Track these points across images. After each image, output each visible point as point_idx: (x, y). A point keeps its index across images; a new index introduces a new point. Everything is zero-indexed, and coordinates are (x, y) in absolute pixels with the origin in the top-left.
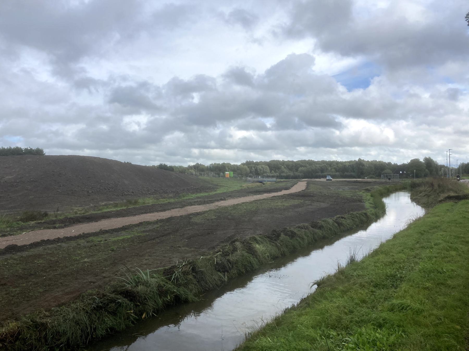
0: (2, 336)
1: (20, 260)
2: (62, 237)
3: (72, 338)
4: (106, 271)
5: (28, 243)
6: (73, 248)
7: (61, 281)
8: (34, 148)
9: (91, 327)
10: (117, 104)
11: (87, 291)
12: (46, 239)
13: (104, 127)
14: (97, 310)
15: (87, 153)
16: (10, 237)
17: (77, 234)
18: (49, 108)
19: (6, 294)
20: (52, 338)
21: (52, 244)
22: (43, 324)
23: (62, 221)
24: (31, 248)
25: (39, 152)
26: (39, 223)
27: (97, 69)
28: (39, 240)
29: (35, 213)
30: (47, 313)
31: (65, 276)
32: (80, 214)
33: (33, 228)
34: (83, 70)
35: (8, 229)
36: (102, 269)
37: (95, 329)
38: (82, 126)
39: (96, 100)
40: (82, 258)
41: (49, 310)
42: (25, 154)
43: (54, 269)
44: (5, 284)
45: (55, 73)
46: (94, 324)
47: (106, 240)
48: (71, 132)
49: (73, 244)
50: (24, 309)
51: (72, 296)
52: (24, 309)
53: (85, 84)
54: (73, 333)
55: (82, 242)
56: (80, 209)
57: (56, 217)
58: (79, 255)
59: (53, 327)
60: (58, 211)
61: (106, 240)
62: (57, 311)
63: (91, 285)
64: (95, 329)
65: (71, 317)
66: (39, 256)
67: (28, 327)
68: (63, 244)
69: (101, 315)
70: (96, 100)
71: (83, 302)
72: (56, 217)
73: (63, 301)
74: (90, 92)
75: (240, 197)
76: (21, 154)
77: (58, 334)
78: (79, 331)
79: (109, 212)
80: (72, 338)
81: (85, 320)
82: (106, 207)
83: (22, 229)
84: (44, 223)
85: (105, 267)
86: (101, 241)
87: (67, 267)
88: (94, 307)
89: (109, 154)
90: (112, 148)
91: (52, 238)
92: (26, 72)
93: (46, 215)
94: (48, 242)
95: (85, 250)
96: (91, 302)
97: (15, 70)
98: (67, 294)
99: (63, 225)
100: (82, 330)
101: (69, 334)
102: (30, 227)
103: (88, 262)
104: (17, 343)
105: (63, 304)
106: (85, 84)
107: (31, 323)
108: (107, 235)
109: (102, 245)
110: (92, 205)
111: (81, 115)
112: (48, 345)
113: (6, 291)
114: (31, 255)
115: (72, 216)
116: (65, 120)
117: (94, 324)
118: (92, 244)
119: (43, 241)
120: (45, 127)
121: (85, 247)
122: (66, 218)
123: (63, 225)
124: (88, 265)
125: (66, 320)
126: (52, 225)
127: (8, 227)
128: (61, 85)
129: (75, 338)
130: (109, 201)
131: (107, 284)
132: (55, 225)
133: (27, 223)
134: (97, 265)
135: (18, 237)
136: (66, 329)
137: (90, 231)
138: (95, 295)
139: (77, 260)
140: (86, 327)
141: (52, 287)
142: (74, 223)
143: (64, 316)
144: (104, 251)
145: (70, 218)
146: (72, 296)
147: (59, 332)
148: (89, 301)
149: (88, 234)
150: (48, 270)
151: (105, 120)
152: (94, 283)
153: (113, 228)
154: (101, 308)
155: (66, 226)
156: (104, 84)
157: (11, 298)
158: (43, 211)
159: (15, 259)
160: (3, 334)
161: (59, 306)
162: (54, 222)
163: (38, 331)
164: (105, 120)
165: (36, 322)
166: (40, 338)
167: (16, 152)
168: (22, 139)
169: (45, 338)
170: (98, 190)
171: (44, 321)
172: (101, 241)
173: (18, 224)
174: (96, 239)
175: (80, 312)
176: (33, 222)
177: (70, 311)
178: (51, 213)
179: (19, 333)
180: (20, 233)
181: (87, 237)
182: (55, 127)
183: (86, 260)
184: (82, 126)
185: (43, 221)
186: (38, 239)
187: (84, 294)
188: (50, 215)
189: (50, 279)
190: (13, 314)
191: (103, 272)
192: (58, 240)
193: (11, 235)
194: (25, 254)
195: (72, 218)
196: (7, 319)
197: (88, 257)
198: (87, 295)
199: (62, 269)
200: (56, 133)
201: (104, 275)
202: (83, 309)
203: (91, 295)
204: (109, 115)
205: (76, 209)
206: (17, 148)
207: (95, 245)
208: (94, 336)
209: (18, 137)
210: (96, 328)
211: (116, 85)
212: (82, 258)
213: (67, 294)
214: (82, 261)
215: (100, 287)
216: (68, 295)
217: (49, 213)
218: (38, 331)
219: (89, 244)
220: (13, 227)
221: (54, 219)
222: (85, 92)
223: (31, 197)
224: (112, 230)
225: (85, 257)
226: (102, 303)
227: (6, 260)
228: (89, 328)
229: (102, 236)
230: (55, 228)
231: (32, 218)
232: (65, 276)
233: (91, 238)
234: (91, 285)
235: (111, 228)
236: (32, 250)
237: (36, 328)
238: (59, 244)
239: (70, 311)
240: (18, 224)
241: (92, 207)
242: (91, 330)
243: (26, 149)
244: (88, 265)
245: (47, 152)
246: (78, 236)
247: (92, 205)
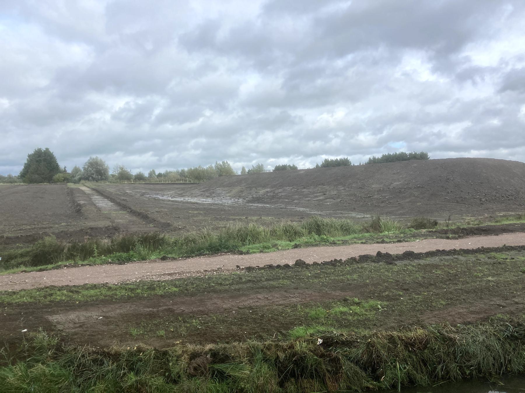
0: (411, 340)
1: (419, 268)
2: (458, 249)
3: (483, 363)
4: (518, 296)
5: (424, 251)
6: (472, 263)
7: (464, 297)
8: (418, 152)
9: (505, 358)
10: (508, 92)
11: (496, 314)
12: (441, 249)
13: (495, 122)
14: (512, 340)
15: (474, 154)
16: (405, 243)
17: (475, 247)
18: (432, 109)
19: (410, 299)
20: (462, 356)
21: (448, 255)
22: (451, 339)
23: (454, 232)
24: (427, 257)
25: (423, 157)
26: (430, 232)
27: (481, 55)
28: (434, 250)
29: (425, 222)
30: (453, 329)
31: (467, 292)
32: (473, 224)
33: (425, 236)
34: (468, 59)
35: (402, 235)
36: (512, 293)
37: (510, 361)
38: (466, 124)
39: (484, 91)
40: (484, 275)
41: (455, 326)
42: (409, 159)
43: (454, 282)
44: (408, 290)
45: (435, 70)
46: (508, 355)
47: (513, 259)
48: (454, 132)
49: (471, 258)
50: (429, 318)
51: (478, 316)
52: (429, 318)
53: (469, 75)
54: (484, 359)
55: (482, 257)
56: (473, 218)
57: (447, 226)
58: (481, 271)
59: (461, 345)
60: (449, 220)
61: (513, 259)
62: (464, 329)
63: (500, 309)
64: (510, 361)
65: (481, 340)
66: (436, 266)
67: (436, 338)
68: (460, 257)
69: (516, 347)
70: (484, 91)
71: (493, 326)
72: (447, 226)
73: (469, 320)
74: (474, 83)
75: (73, 290)
76: (405, 160)
77: (467, 355)
78: (491, 359)
79: (510, 225)
80: (483, 363)
81: (498, 348)
82: (505, 219)
83: (415, 236)
84: (435, 232)
85: (516, 291)
86: (507, 259)
87: (468, 283)
88: (507, 335)
89: (502, 154)
90: (507, 147)
91: (448, 249)
92: (406, 74)
93: (436, 223)
94: (443, 252)
95: (486, 266)
96: (503, 328)
97: (398, 75)
98: (472, 313)
99: (457, 236)
100: (494, 358)
101: (480, 358)
102: (422, 235)
103: (492, 281)
104: (426, 351)
105: (469, 323)
106: (469, 75)
107: (439, 334)
108: (513, 252)
109: (508, 263)
110: (486, 215)
111: (466, 111)
112: (457, 363)
113: (409, 296)
114: (428, 265)
115: (465, 227)
116: (447, 119)
117: (508, 355)
118: (495, 260)
119: (438, 251)
120: (426, 130)
121: (486, 264)
122: (459, 228)
123: (457, 236)
124: (493, 285)
125: (476, 341)
126: (444, 234)
127: (401, 233)
128: (442, 81)
129: (486, 364)
130: (509, 211)
131: (521, 311)
132: (448, 235)
133: (419, 231)
134: (505, 286)
135: (412, 243)
136: (476, 351)
137: (491, 246)
138: (507, 321)
139: (477, 277)
140: (500, 356)
141: (455, 302)
142: (468, 234)
143: (473, 337)
144: (512, 272)
145: (463, 229)
146: (478, 316)
147: (468, 353)
148: (502, 328)
149: (488, 248)
150: (448, 283)
151: (495, 113)
152: (503, 307)
153: (521, 244)
154: (517, 338)
155: (460, 237)
156: (493, 70)
157: (415, 304)
158: (433, 219)
159: (413, 266)
160: (412, 338)
161: (466, 324)
162: (446, 232)
163: (446, 345)
164: (495, 113)
165: (443, 335)
166: (449, 352)
167: (401, 158)
168: (405, 144)
169: (454, 353)
170: (493, 197)
171: (452, 336)
172: (507, 259)
173: (411, 231)
174: (500, 256)
175: (491, 337)
176: (424, 230)
177: (479, 333)
178: (441, 221)
179: (427, 342)
180: (414, 241)
181: (488, 252)
182: (437, 128)
183: (490, 278)
184: (466, 124)
185: (434, 230)
186: (434, 249)
187: (493, 318)
188: (440, 224)
189: (451, 293)
190: (419, 321)
191: (514, 297)
192: (454, 252)
193: (406, 241)
194: (422, 262)
195: (465, 229)
196: (413, 324)
197: (493, 276)
198: (497, 320)
199: (463, 284)
200: (439, 135)
201: (516, 300)
202: (494, 334)
203: (502, 320)
204: (501, 106)
205: (468, 219)
206: (402, 153)
207: (500, 263)
208: (509, 369)
209: (401, 142)
210: (510, 360)
211: (509, 68)
212: (484, 275)
213: (472, 313)
214: (485, 279)
215: (512, 313)
216: (474, 314)
217: (439, 222)
218: (446, 345)
219: (491, 261)
220: (406, 233)
221: (445, 228)
222: (468, 84)
223: (418, 204)
224: (519, 247)
225: (489, 275)
226: (517, 332)
227: (406, 265)
228: (503, 358)
229: (507, 253)
230: (448, 238)
231: (420, 226)
232: (467, 292)
233: (493, 254)
234: (500, 309)
235: (516, 245)
236: (428, 259)
237: (445, 341)
238: (456, 256)
239: (479, 333)
240: (411, 231)
241: (487, 218)
242: (505, 360)
243: (410, 154)
244: (493, 285)
245: (432, 156)
246: (476, 250)
247: (486, 215)
